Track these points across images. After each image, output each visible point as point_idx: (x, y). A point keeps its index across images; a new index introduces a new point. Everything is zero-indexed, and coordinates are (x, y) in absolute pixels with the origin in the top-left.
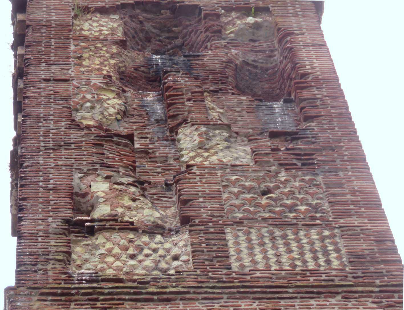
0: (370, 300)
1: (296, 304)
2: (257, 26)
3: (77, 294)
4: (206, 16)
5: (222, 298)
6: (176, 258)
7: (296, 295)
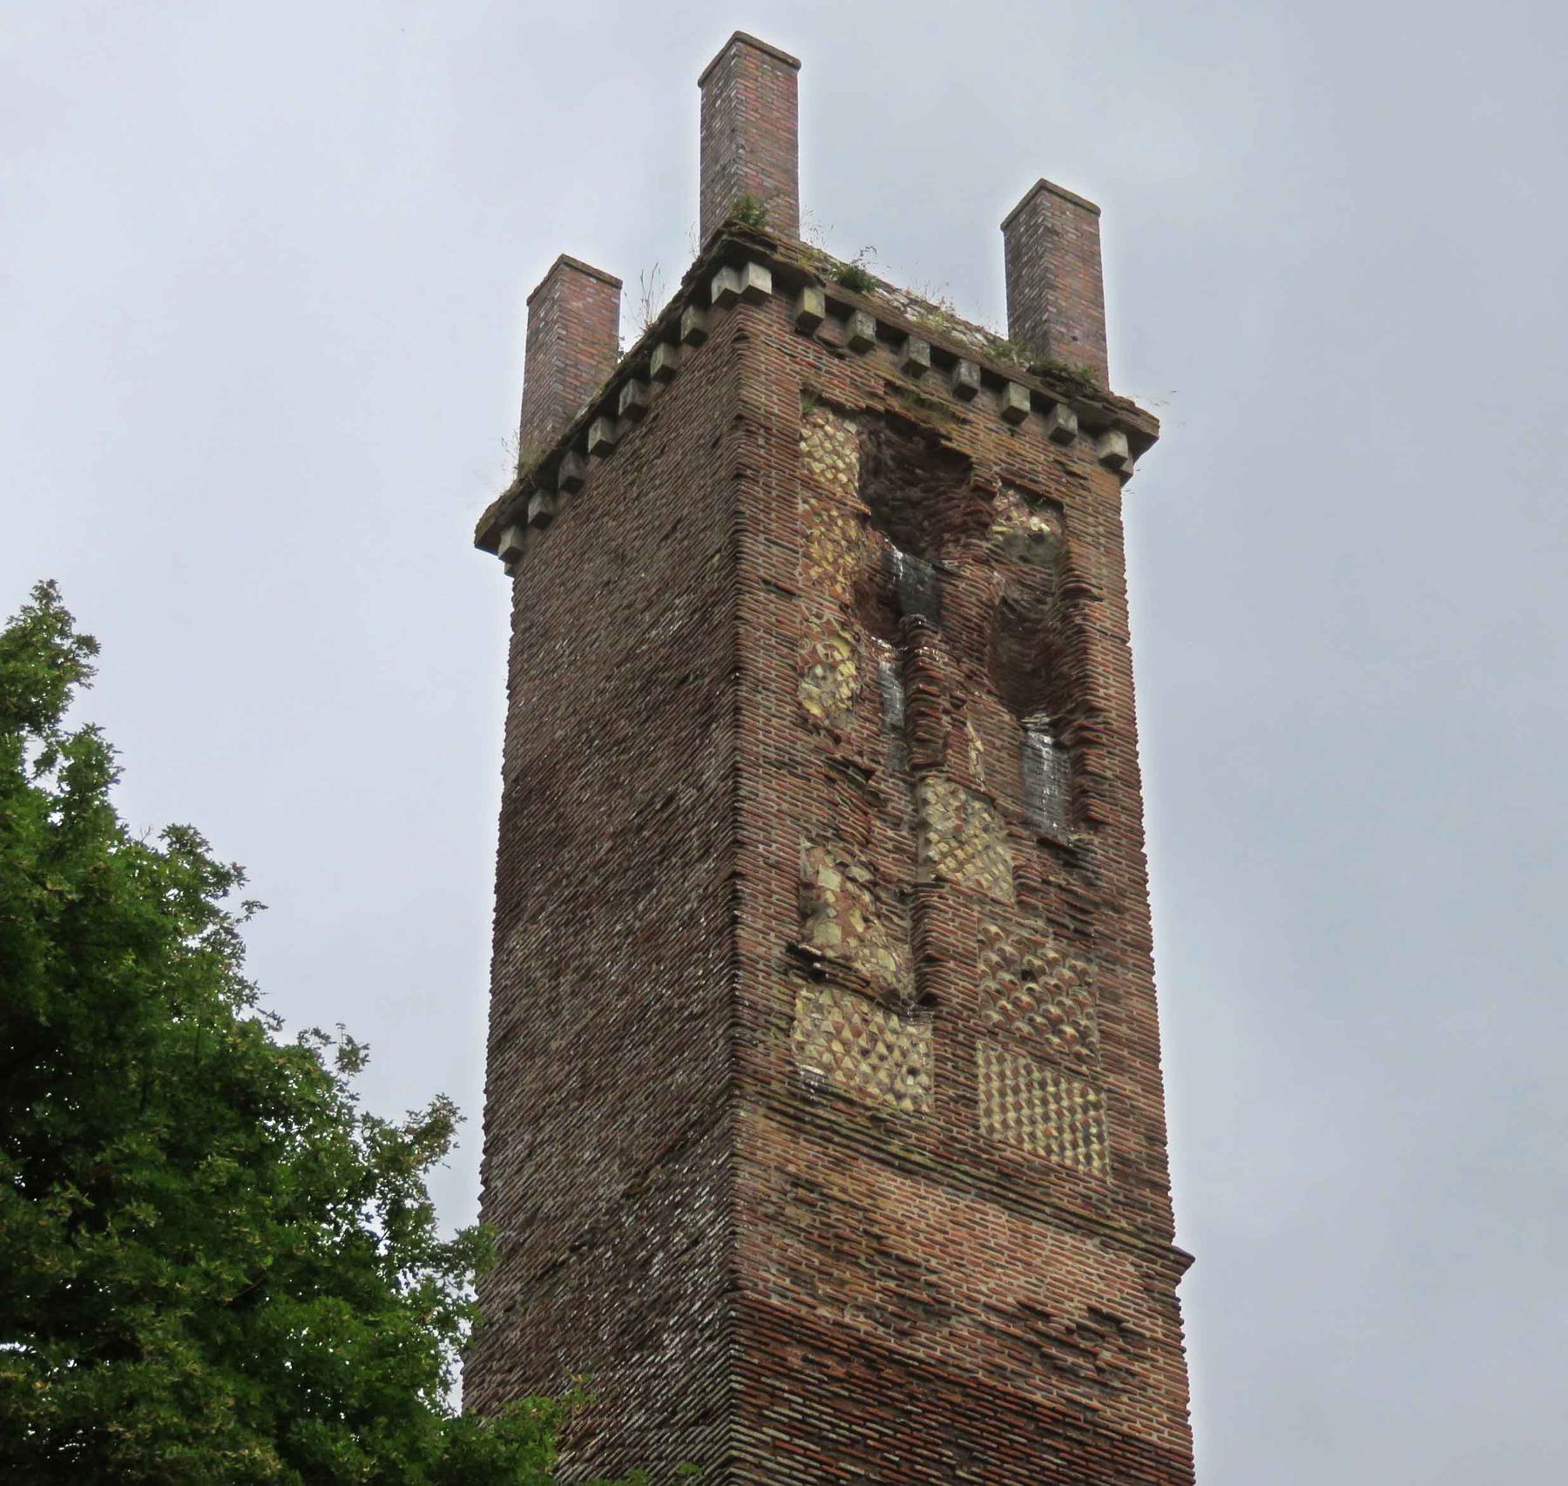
0: (1131, 1258)
1: (1049, 1234)
3: (810, 1123)
5: (969, 1193)
6: (913, 1072)
7: (1051, 1220)
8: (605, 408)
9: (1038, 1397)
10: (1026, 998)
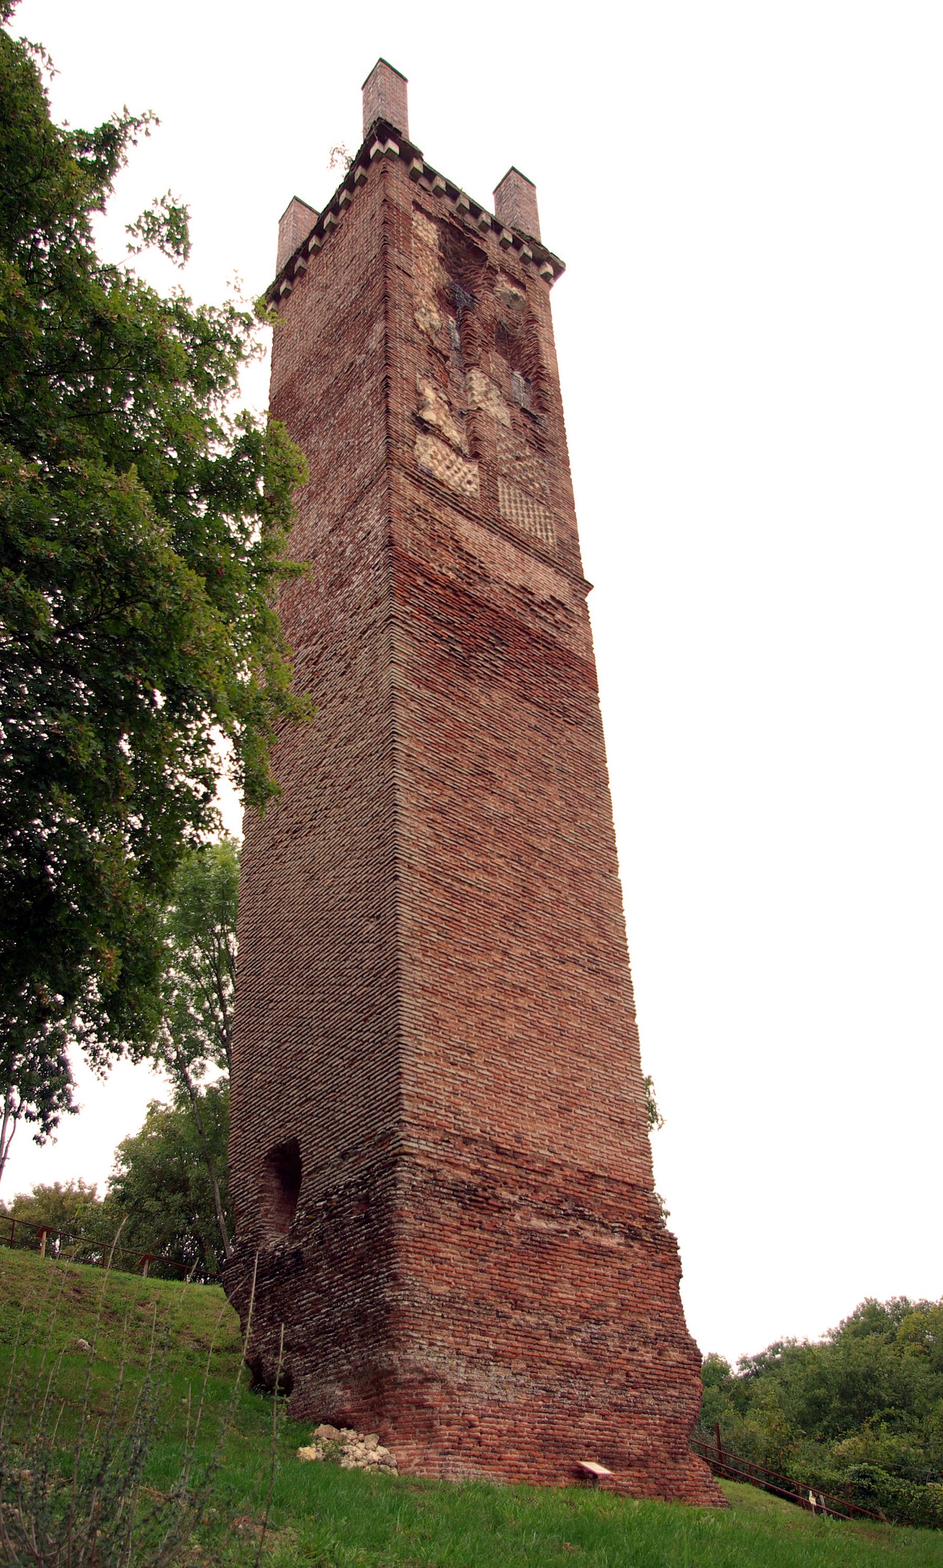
2: (516, 297)
4: (490, 268)
6: (469, 482)
8: (318, 231)
9: (530, 625)
10: (518, 467)
